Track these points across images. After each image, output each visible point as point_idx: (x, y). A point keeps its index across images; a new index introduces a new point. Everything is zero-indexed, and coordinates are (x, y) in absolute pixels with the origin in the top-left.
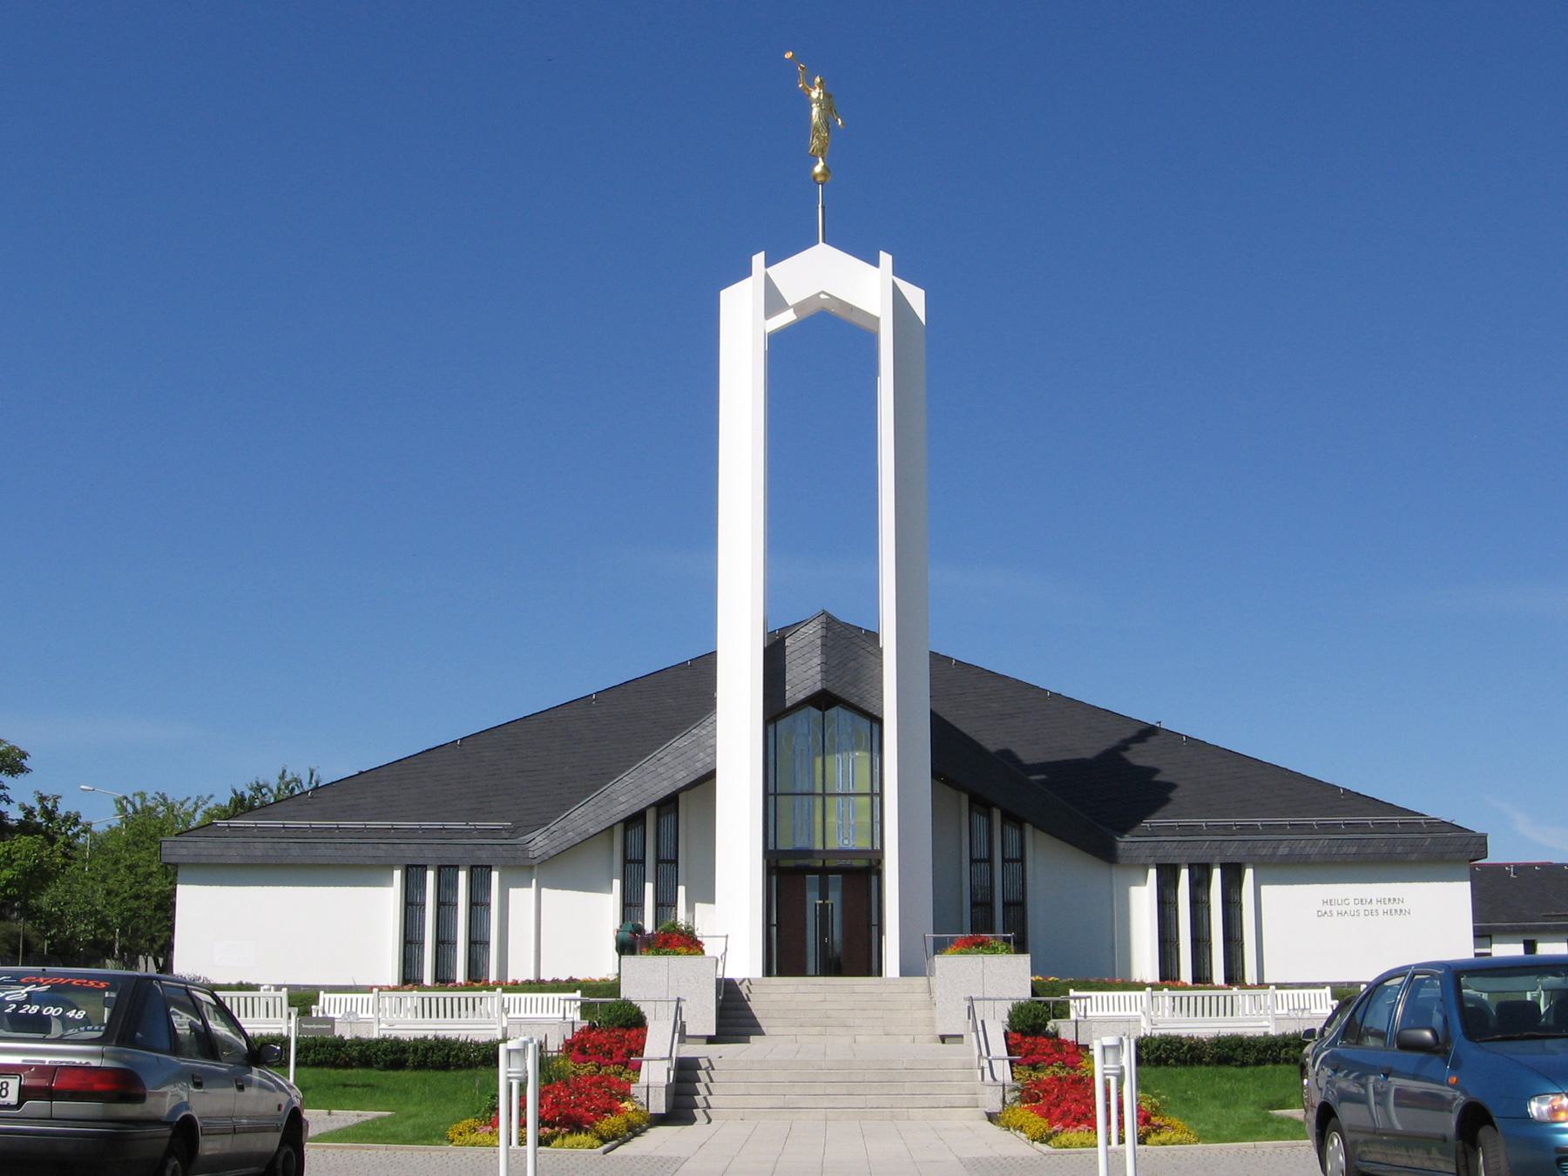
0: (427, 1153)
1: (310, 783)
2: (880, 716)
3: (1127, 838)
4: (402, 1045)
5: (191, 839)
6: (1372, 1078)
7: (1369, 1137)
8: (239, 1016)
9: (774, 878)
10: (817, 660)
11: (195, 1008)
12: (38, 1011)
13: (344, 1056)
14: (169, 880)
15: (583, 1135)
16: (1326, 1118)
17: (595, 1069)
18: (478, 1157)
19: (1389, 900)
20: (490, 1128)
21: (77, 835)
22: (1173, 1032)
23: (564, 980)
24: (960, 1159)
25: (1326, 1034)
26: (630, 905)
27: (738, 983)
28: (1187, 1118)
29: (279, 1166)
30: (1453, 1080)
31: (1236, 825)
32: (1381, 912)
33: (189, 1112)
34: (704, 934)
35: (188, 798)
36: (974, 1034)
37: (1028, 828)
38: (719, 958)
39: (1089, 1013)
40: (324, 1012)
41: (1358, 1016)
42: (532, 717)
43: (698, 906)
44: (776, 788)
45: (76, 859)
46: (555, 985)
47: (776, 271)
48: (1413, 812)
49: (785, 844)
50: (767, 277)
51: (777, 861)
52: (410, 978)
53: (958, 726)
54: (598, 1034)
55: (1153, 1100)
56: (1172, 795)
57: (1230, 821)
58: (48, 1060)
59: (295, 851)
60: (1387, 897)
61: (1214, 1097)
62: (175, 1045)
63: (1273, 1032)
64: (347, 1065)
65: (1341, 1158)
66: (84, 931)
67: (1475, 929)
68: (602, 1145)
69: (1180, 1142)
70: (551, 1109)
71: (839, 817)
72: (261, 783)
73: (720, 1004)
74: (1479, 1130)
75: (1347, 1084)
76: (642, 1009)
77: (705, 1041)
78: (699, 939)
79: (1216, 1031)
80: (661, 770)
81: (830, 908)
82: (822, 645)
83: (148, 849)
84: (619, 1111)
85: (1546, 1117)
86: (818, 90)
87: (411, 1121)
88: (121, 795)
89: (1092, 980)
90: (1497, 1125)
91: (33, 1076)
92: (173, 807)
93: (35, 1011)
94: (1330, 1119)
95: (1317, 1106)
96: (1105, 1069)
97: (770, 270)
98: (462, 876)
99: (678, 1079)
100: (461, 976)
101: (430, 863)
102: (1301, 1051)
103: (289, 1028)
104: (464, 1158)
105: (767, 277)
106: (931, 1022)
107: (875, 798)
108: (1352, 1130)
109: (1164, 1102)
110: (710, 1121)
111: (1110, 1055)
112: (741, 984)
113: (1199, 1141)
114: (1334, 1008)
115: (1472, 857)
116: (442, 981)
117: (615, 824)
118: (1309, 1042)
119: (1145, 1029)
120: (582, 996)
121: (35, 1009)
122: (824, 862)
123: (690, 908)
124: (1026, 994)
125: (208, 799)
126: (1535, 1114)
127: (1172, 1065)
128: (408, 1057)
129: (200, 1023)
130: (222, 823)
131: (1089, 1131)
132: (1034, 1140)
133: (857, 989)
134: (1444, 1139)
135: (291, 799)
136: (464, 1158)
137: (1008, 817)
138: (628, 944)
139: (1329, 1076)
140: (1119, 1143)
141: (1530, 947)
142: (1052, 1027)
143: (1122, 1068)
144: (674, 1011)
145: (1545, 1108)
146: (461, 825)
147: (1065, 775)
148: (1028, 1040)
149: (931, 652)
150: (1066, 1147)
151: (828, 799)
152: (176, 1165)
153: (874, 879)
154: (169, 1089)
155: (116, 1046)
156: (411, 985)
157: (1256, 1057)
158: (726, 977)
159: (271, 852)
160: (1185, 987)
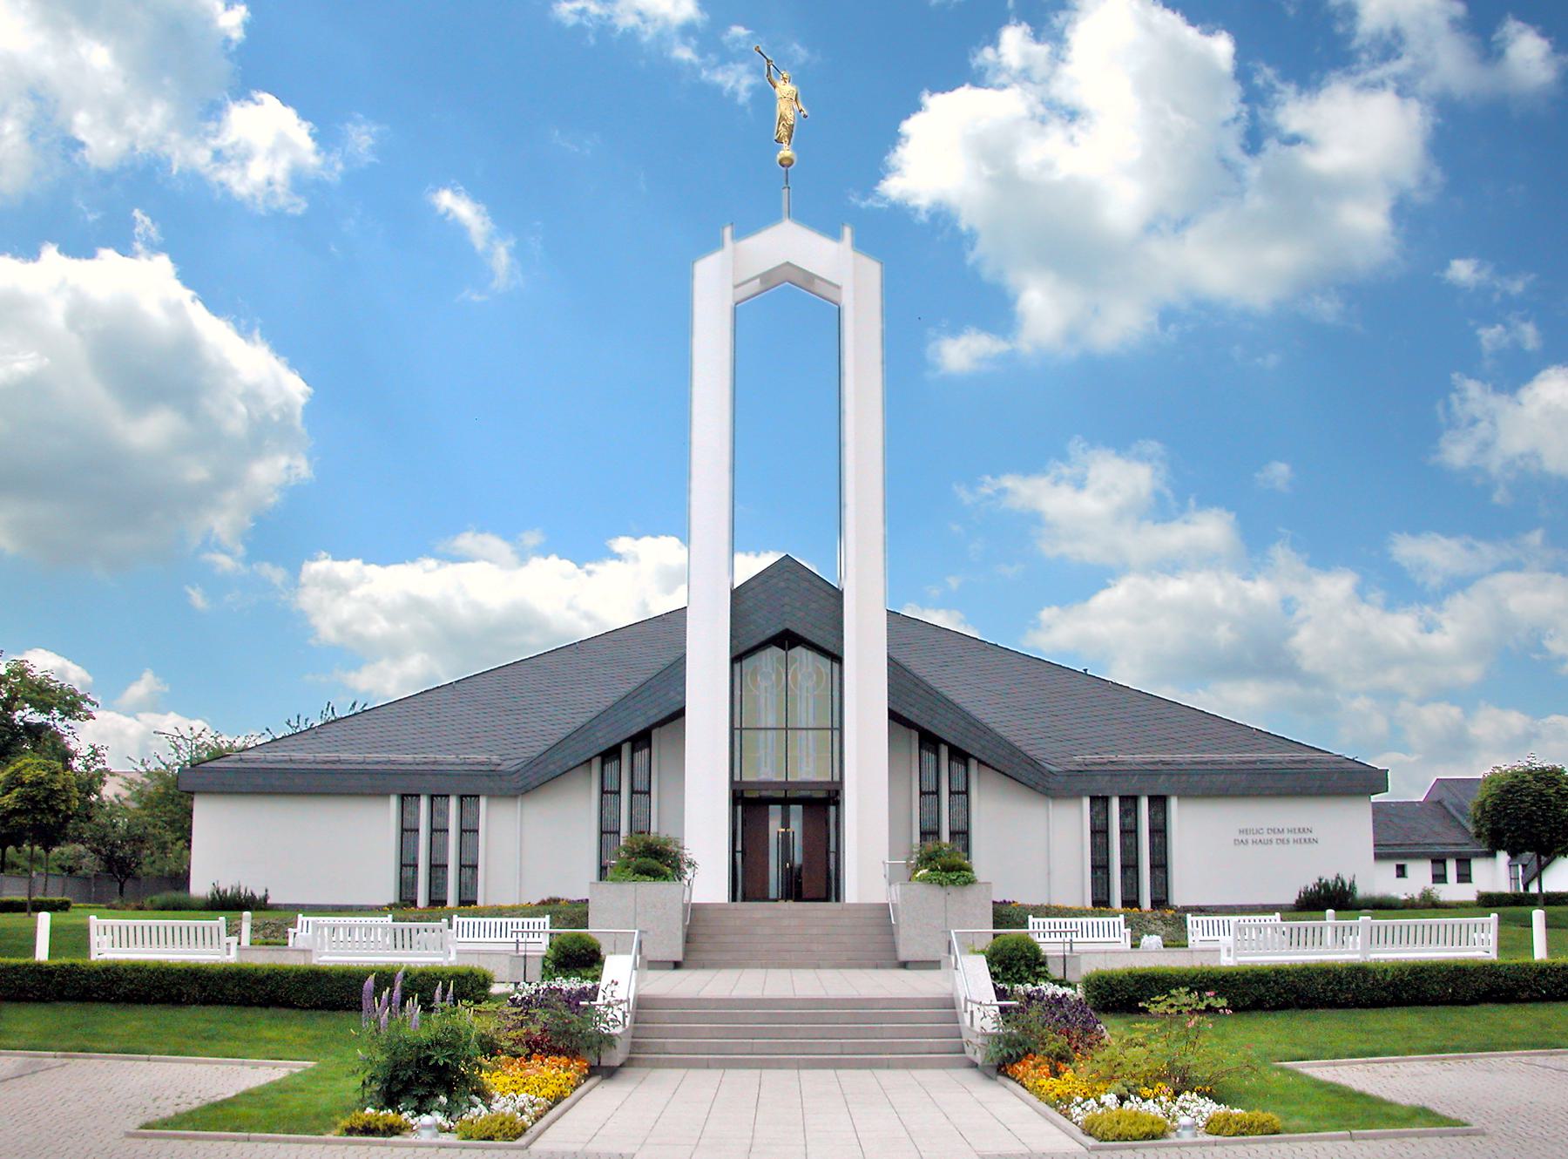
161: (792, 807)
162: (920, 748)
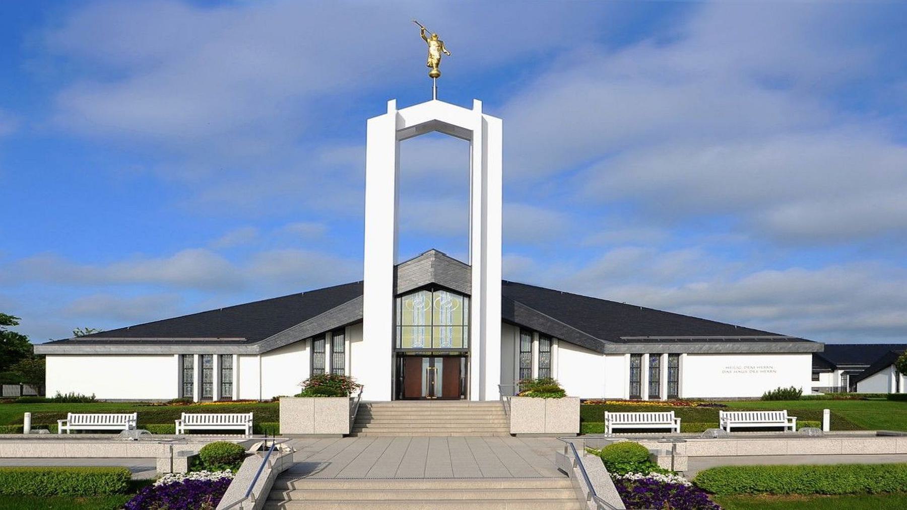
67: (813, 371)
97: (402, 112)
122: (432, 353)
161: (436, 358)
162: (521, 333)
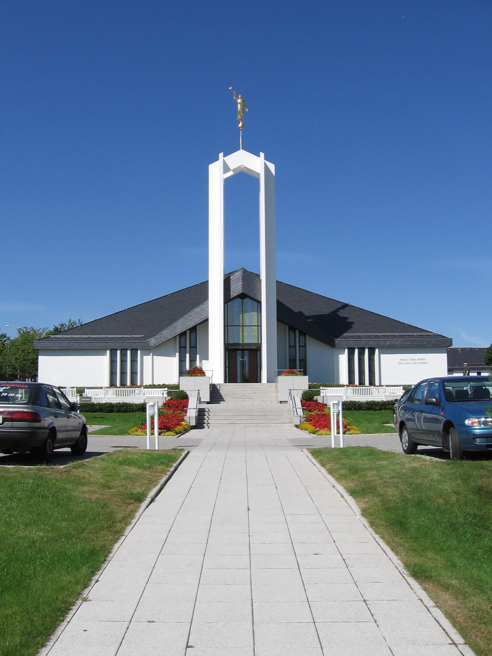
0: (122, 438)
1: (79, 323)
2: (260, 301)
3: (338, 339)
4: (113, 405)
5: (42, 341)
6: (416, 413)
7: (415, 431)
8: (68, 396)
9: (227, 352)
10: (241, 284)
11: (54, 394)
12: (7, 395)
13: (94, 408)
14: (35, 354)
15: (171, 432)
16: (402, 425)
17: (173, 412)
18: (138, 439)
19: (421, 359)
20: (142, 430)
21: (5, 341)
22: (354, 400)
23: (161, 384)
24: (287, 439)
25: (401, 401)
26: (182, 361)
27: (216, 385)
28: (357, 427)
29: (80, 442)
30: (442, 414)
31: (373, 335)
32: (418, 363)
33: (53, 425)
34: (206, 370)
35: (40, 329)
36: (291, 401)
37: (307, 336)
38: (210, 377)
39: (327, 394)
40: (86, 395)
41: (412, 395)
42: (150, 302)
43: (203, 361)
44: (227, 324)
45: (5, 348)
46: (159, 386)
47: (227, 159)
48: (429, 331)
49: (231, 342)
50: (224, 160)
51: (228, 347)
52: (113, 384)
53: (285, 304)
54: (174, 401)
55: (348, 421)
56: (352, 326)
57: (371, 334)
58: (11, 410)
59: (76, 345)
60: (420, 358)
61: (366, 420)
62: (49, 405)
63: (384, 400)
64: (95, 411)
65: (407, 438)
66: (9, 371)
67: (448, 368)
68: (176, 435)
69: (356, 434)
70: (160, 424)
71: (247, 333)
72: (63, 324)
73: (211, 392)
74: (449, 429)
75: (408, 416)
76: (187, 393)
77: (206, 403)
78: (204, 371)
79: (367, 400)
80: (191, 318)
81: (245, 361)
82: (242, 279)
83: (28, 345)
84: (181, 425)
85: (470, 425)
86: (240, 100)
87: (117, 428)
88: (19, 328)
89: (327, 384)
90: (455, 427)
91: (7, 415)
92: (36, 332)
93: (6, 395)
94: (403, 426)
95: (399, 422)
96: (334, 410)
97: (224, 158)
98: (129, 352)
99: (199, 415)
100: (129, 383)
101: (118, 348)
102: (393, 406)
103: (77, 400)
104: (134, 439)
105: (224, 160)
106: (277, 397)
107: (259, 327)
108: (411, 429)
109: (351, 421)
110: (209, 428)
111: (335, 406)
112: (217, 385)
113: (362, 433)
114: (404, 393)
115: (447, 346)
116: (123, 385)
117: (177, 336)
118: (396, 403)
119: (344, 399)
120: (168, 389)
121: (6, 394)
122: (243, 347)
123: (201, 362)
124: (307, 388)
125: (47, 329)
126: (467, 424)
127: (353, 410)
128: (114, 409)
129: (56, 400)
130: (52, 336)
131: (328, 430)
132: (310, 433)
133: (254, 387)
134: (439, 432)
135: (73, 329)
136: (134, 439)
137: (301, 333)
138: (182, 373)
139: (403, 413)
140: (337, 434)
141: (479, 373)
142: (315, 399)
143: (339, 410)
144: (197, 394)
145: (470, 422)
146: (128, 336)
147: (319, 319)
148: (308, 402)
149: (277, 281)
150: (320, 435)
151: (244, 327)
152: (50, 441)
153: (259, 352)
154: (47, 418)
155: (32, 405)
156: (113, 387)
157: (379, 408)
158: (213, 383)
159: (68, 345)
160: (357, 386)
